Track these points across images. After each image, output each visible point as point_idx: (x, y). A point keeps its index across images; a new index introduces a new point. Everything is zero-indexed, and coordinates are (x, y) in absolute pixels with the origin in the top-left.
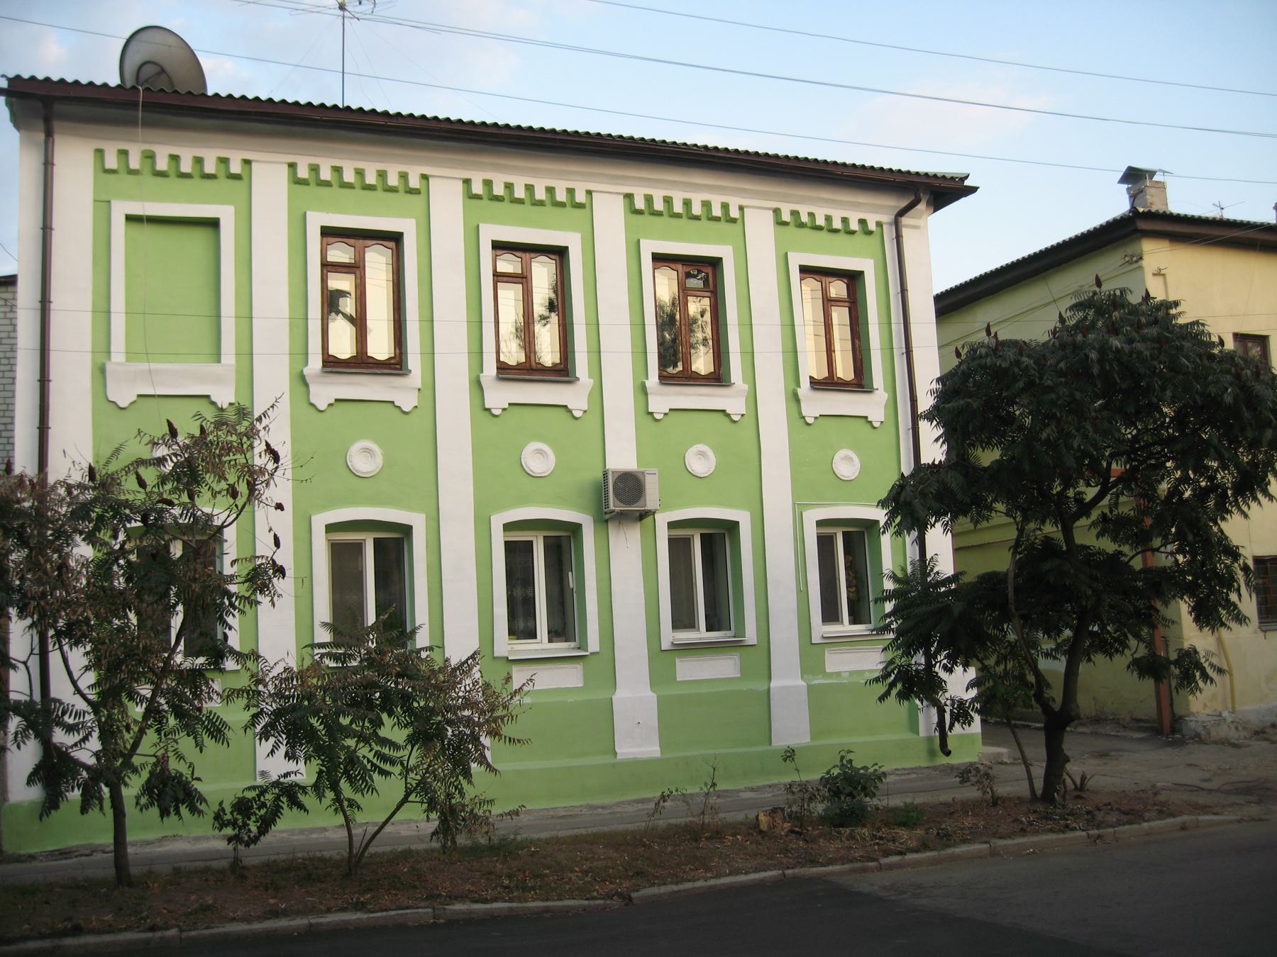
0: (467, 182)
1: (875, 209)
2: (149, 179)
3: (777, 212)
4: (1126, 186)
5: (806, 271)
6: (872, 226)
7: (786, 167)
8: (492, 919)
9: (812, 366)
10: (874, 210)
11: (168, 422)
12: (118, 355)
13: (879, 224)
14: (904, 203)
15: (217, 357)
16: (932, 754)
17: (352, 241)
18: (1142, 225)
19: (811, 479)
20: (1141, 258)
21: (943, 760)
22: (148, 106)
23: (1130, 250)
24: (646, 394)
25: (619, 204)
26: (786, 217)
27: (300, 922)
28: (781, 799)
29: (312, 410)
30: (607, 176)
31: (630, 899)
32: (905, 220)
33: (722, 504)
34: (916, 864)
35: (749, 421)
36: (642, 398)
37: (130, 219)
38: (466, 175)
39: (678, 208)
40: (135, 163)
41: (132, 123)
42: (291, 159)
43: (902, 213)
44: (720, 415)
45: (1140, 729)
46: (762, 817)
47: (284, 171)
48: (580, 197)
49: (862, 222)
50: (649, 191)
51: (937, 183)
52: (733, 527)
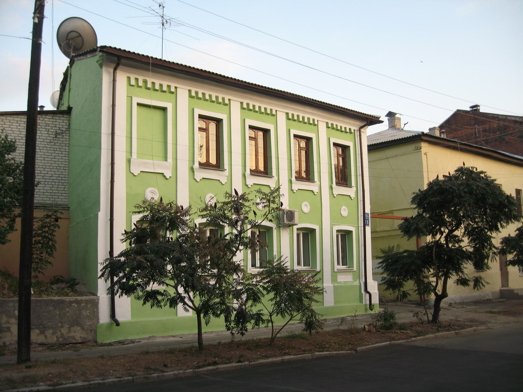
0: (242, 103)
1: (354, 125)
2: (144, 90)
3: (327, 123)
4: (387, 118)
5: (296, 136)
6: (353, 131)
7: (255, 88)
8: (326, 357)
9: (251, 165)
10: (353, 125)
11: (235, 190)
12: (134, 156)
13: (354, 130)
14: (362, 124)
15: (166, 159)
16: (366, 310)
17: (205, 120)
18: (424, 138)
19: (336, 217)
20: (421, 148)
21: (370, 312)
22: (148, 64)
23: (417, 145)
24: (193, 172)
25: (284, 115)
26: (330, 126)
27: (279, 359)
28: (370, 321)
29: (195, 181)
30: (282, 106)
31: (357, 350)
32: (362, 130)
33: (306, 222)
34: (420, 340)
35: (174, 179)
36: (192, 173)
37: (139, 105)
38: (242, 101)
39: (220, 100)
40: (141, 83)
41: (148, 70)
42: (190, 88)
43: (362, 127)
44: (311, 192)
45: (414, 304)
46: (366, 327)
47: (285, 115)
48: (274, 113)
49: (350, 129)
50: (298, 114)
51: (348, 112)
52: (351, 232)
